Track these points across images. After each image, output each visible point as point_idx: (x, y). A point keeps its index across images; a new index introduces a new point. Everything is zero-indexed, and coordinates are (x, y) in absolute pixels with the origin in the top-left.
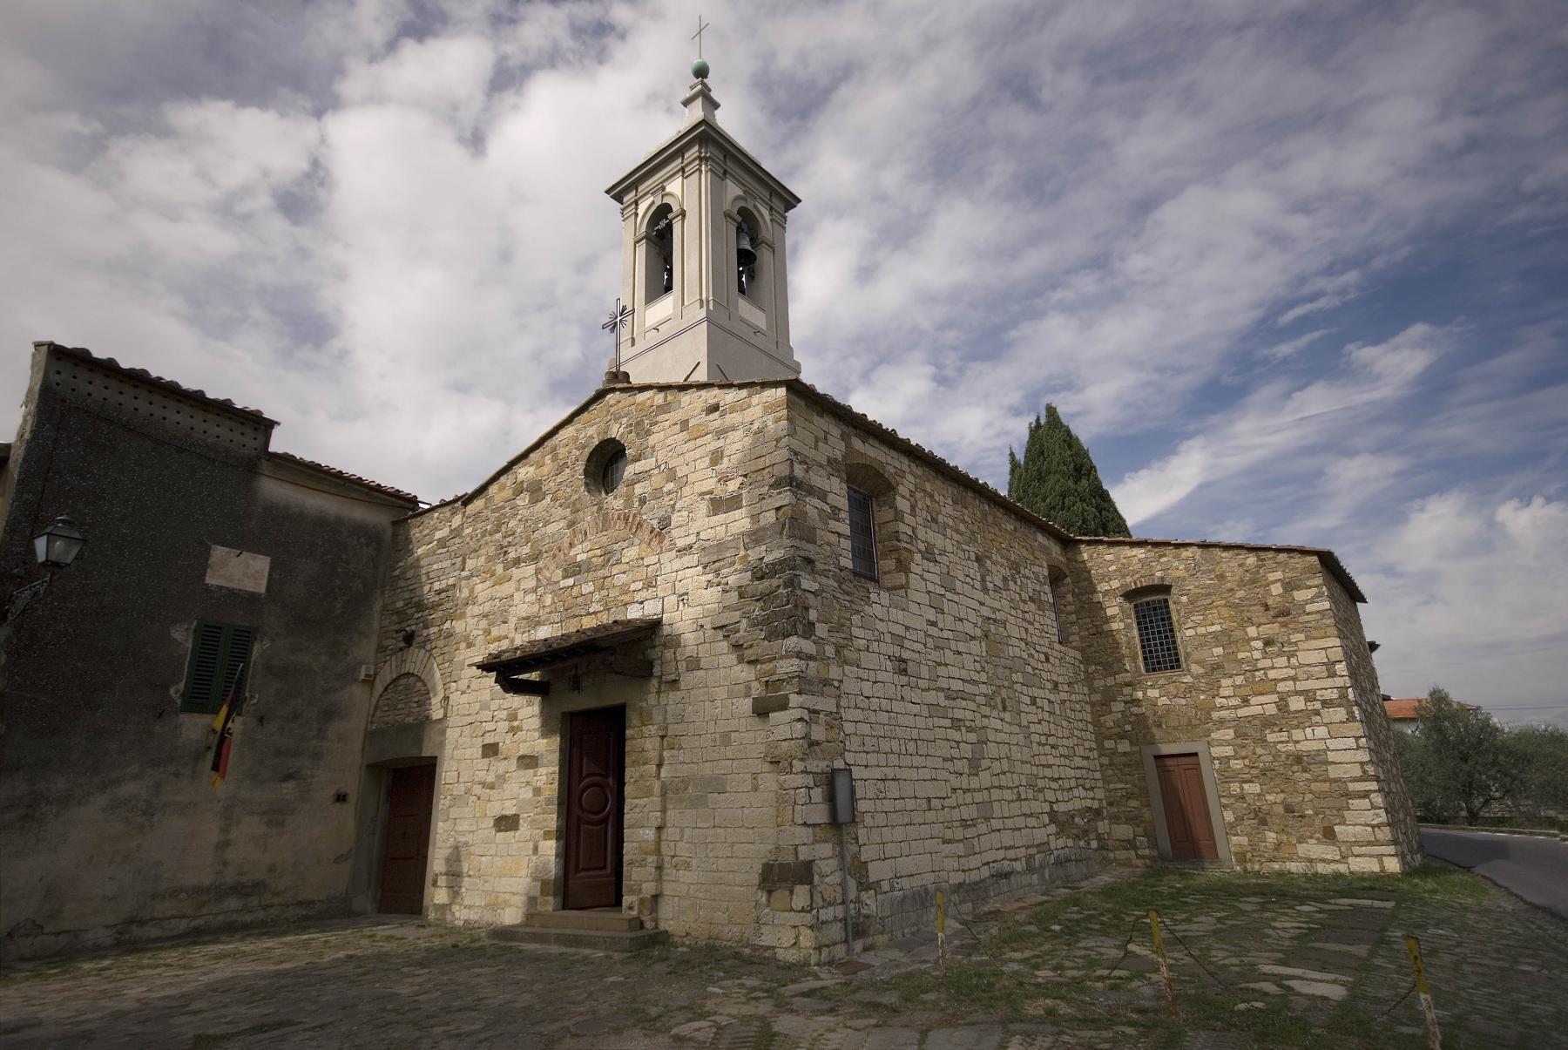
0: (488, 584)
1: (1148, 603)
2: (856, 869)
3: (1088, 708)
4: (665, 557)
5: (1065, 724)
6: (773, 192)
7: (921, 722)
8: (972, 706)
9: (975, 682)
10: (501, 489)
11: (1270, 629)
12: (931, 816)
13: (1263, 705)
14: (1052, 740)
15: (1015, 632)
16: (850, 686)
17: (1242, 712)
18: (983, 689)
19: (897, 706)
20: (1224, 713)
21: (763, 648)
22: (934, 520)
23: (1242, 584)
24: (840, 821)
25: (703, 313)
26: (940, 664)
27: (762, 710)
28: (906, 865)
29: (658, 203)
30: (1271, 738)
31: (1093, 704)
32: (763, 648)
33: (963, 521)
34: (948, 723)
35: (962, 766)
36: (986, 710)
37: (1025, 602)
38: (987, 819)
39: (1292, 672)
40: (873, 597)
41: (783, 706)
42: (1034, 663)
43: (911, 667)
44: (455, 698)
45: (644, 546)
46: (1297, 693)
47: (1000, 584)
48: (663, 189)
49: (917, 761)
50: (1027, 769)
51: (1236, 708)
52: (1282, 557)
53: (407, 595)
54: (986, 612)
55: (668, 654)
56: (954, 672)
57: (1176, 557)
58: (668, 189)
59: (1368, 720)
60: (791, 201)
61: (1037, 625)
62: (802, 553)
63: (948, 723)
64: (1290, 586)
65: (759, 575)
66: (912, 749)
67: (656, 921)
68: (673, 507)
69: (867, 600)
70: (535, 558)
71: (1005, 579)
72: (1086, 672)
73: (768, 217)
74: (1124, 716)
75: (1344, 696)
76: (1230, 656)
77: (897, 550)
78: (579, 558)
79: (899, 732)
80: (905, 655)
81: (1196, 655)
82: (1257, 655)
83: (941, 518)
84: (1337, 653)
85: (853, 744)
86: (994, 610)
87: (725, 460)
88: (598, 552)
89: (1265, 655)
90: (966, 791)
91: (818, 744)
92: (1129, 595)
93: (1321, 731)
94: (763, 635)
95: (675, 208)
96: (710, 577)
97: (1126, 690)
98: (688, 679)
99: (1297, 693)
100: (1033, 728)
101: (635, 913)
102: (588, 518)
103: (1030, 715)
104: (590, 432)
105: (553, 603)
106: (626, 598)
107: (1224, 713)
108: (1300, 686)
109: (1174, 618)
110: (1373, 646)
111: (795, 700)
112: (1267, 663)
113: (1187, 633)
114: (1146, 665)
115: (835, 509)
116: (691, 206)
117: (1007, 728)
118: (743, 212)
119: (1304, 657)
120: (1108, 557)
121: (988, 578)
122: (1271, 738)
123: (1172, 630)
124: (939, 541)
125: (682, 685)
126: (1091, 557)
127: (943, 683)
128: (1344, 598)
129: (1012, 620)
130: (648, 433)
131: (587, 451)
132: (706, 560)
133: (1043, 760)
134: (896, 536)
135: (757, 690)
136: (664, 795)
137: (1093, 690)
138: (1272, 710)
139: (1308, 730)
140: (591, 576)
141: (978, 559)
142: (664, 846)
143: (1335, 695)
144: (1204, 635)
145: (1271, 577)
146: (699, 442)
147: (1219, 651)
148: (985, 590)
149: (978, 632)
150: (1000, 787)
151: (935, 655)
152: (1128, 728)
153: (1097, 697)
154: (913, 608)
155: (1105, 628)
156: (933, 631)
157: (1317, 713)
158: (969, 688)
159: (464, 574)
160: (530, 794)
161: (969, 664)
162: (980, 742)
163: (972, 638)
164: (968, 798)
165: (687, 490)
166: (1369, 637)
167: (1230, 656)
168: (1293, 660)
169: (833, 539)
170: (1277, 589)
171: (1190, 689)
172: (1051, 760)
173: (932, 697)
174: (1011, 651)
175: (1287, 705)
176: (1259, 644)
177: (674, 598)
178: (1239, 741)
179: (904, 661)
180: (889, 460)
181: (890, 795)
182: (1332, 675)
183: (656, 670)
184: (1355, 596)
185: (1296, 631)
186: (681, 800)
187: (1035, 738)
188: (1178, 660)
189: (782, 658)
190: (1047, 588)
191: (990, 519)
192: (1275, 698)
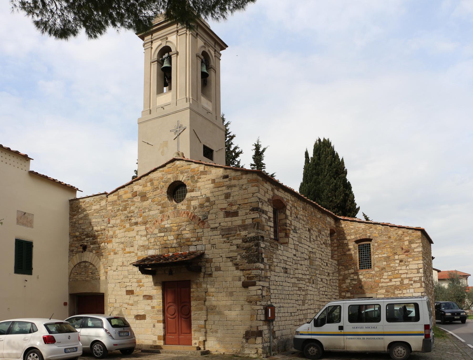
0: (122, 231)
1: (363, 245)
2: (273, 333)
3: (338, 281)
4: (205, 230)
5: (330, 287)
6: (216, 42)
7: (290, 289)
8: (304, 283)
9: (305, 275)
10: (126, 193)
11: (403, 257)
12: (291, 318)
13: (396, 282)
14: (326, 293)
15: (318, 256)
16: (272, 278)
17: (389, 284)
18: (308, 277)
19: (284, 284)
20: (383, 284)
21: (246, 266)
22: (297, 217)
23: (396, 240)
24: (269, 320)
25: (188, 105)
26: (296, 269)
27: (245, 285)
28: (284, 332)
29: (164, 45)
30: (397, 292)
31: (339, 280)
32: (246, 266)
33: (305, 216)
34: (297, 289)
35: (300, 302)
36: (308, 284)
37: (322, 244)
38: (306, 319)
39: (406, 271)
40: (279, 247)
41: (254, 284)
42: (323, 267)
43: (288, 270)
44: (110, 273)
45: (196, 225)
46: (407, 278)
47: (315, 238)
48: (167, 38)
49: (289, 301)
50: (318, 303)
51: (387, 282)
52: (410, 231)
53: (80, 230)
54: (310, 249)
55: (208, 265)
56: (300, 271)
57: (376, 229)
58: (169, 39)
59: (427, 285)
60: (223, 46)
61: (325, 253)
62: (260, 234)
63: (297, 289)
64: (411, 242)
65: (245, 241)
66: (287, 298)
67: (204, 348)
68: (209, 212)
69: (277, 249)
70: (145, 223)
71: (316, 237)
72: (338, 269)
73: (213, 55)
74: (350, 285)
75: (420, 280)
76: (388, 265)
77: (286, 230)
78: (166, 226)
79: (285, 292)
80: (287, 267)
81: (377, 264)
82: (397, 265)
83: (299, 216)
84: (421, 266)
85: (273, 296)
86: (313, 248)
87: (231, 198)
88: (175, 225)
89: (399, 265)
90: (301, 310)
91: (264, 296)
92: (357, 242)
93: (412, 291)
94: (246, 261)
95: (173, 50)
96: (225, 239)
97: (352, 276)
98: (215, 274)
99: (407, 278)
100: (321, 289)
101: (197, 345)
102: (170, 211)
103: (320, 284)
104: (170, 177)
105: (155, 241)
106: (189, 243)
107: (383, 284)
108: (408, 276)
109: (372, 250)
110: (433, 258)
111: (258, 283)
112: (399, 268)
113: (376, 256)
114: (360, 267)
115: (270, 218)
116: (181, 50)
117: (313, 290)
118: (204, 54)
119: (411, 266)
120: (351, 227)
121: (312, 237)
122: (397, 292)
123: (370, 255)
124: (298, 225)
125: (214, 276)
126: (345, 226)
127: (297, 276)
128: (426, 241)
129: (317, 251)
130: (197, 182)
131: (168, 184)
132: (223, 233)
133: (323, 300)
134: (285, 224)
135: (243, 279)
136: (207, 310)
137: (340, 275)
138: (398, 283)
139: (408, 290)
140: (172, 233)
141: (309, 230)
142: (207, 326)
143: (418, 279)
144: (381, 257)
145: (406, 238)
146: (220, 189)
147: (385, 263)
148: (310, 241)
149: (307, 257)
150: (310, 309)
151: (295, 266)
152: (351, 288)
153: (341, 277)
154: (290, 250)
155: (348, 253)
156: (295, 258)
157: (412, 285)
158: (304, 277)
159: (109, 225)
160: (150, 308)
161: (304, 269)
162: (306, 295)
163: (306, 259)
164: (301, 312)
165: (214, 207)
166: (433, 255)
167: (388, 265)
168: (408, 267)
169: (269, 228)
170: (406, 243)
171: (373, 276)
172: (325, 300)
173: (294, 280)
174: (317, 263)
175: (403, 282)
176: (398, 261)
177: (210, 246)
178: (386, 293)
179: (286, 269)
180: (285, 197)
181: (281, 312)
182: (418, 272)
183: (203, 270)
184: (431, 242)
185: (410, 257)
186: (214, 312)
187: (321, 293)
188: (371, 266)
189: (254, 269)
190: (329, 238)
191: (313, 214)
192: (400, 279)
